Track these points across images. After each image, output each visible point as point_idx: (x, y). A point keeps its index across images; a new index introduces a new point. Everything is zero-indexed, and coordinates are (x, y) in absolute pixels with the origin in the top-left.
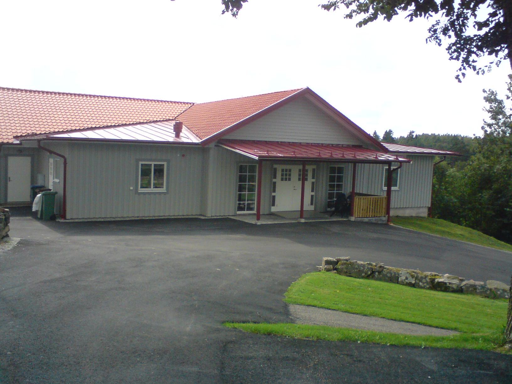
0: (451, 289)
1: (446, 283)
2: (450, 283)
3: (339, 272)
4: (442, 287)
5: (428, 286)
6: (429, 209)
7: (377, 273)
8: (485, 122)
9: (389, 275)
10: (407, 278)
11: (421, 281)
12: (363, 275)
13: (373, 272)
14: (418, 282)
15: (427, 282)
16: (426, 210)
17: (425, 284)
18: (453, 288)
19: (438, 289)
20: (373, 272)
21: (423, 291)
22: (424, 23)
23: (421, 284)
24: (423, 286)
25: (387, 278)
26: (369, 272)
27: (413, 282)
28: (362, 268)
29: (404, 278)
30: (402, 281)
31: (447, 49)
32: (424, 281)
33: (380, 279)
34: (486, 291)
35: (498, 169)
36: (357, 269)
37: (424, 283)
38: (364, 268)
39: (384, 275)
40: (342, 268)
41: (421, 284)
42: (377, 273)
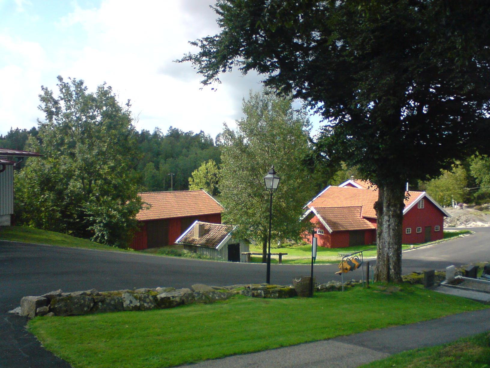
0: (175, 303)
1: (169, 298)
2: (173, 297)
3: (57, 313)
4: (165, 304)
5: (153, 306)
6: (12, 216)
7: (100, 304)
8: (40, 122)
9: (113, 303)
10: (131, 302)
11: (145, 301)
12: (85, 309)
13: (96, 303)
14: (142, 303)
15: (151, 301)
16: (8, 218)
17: (150, 304)
18: (176, 301)
19: (163, 306)
20: (96, 303)
21: (150, 313)
22: (234, 127)
23: (145, 304)
24: (148, 306)
25: (111, 307)
26: (92, 304)
27: (138, 304)
28: (83, 301)
29: (128, 302)
30: (128, 307)
31: (81, 83)
32: (148, 300)
33: (104, 311)
34: (202, 297)
35: (64, 170)
36: (77, 303)
37: (148, 303)
38: (85, 301)
39: (109, 304)
40: (60, 307)
41: (145, 304)
42: (100, 304)
